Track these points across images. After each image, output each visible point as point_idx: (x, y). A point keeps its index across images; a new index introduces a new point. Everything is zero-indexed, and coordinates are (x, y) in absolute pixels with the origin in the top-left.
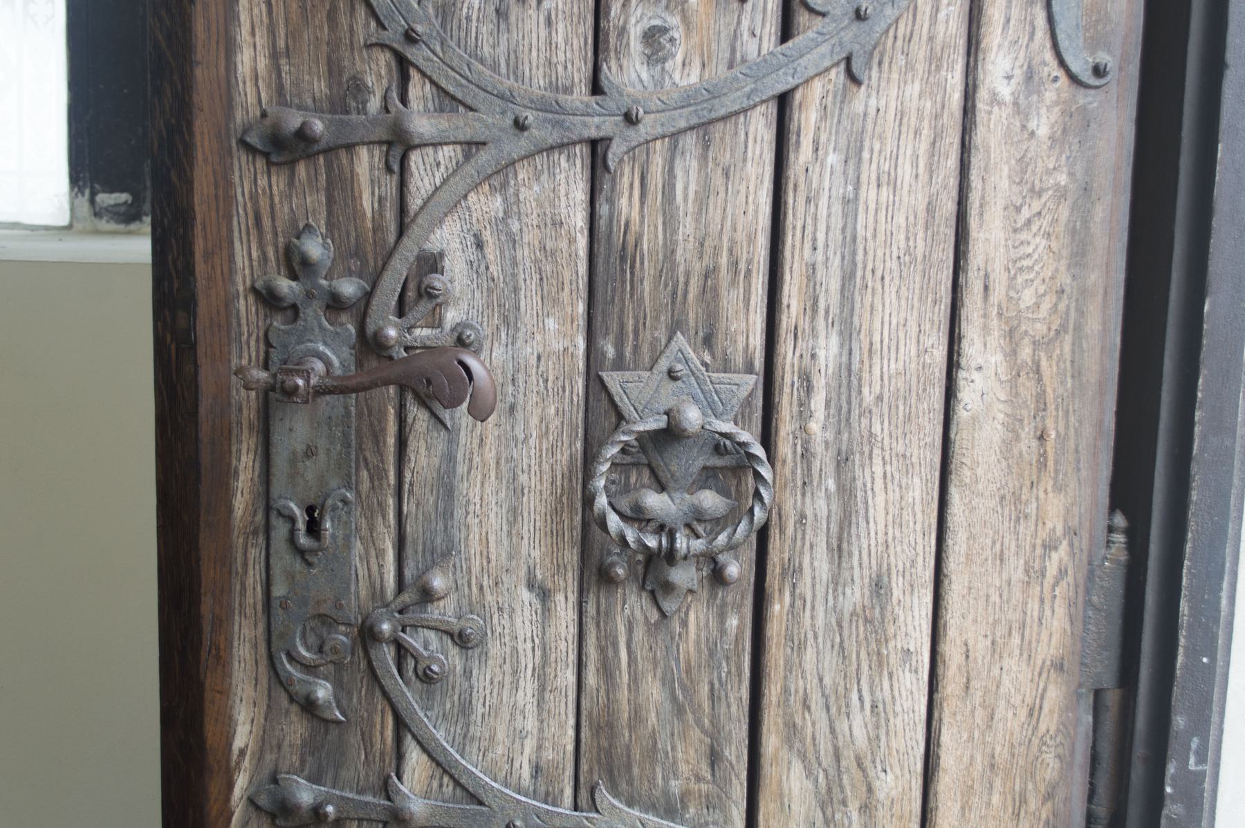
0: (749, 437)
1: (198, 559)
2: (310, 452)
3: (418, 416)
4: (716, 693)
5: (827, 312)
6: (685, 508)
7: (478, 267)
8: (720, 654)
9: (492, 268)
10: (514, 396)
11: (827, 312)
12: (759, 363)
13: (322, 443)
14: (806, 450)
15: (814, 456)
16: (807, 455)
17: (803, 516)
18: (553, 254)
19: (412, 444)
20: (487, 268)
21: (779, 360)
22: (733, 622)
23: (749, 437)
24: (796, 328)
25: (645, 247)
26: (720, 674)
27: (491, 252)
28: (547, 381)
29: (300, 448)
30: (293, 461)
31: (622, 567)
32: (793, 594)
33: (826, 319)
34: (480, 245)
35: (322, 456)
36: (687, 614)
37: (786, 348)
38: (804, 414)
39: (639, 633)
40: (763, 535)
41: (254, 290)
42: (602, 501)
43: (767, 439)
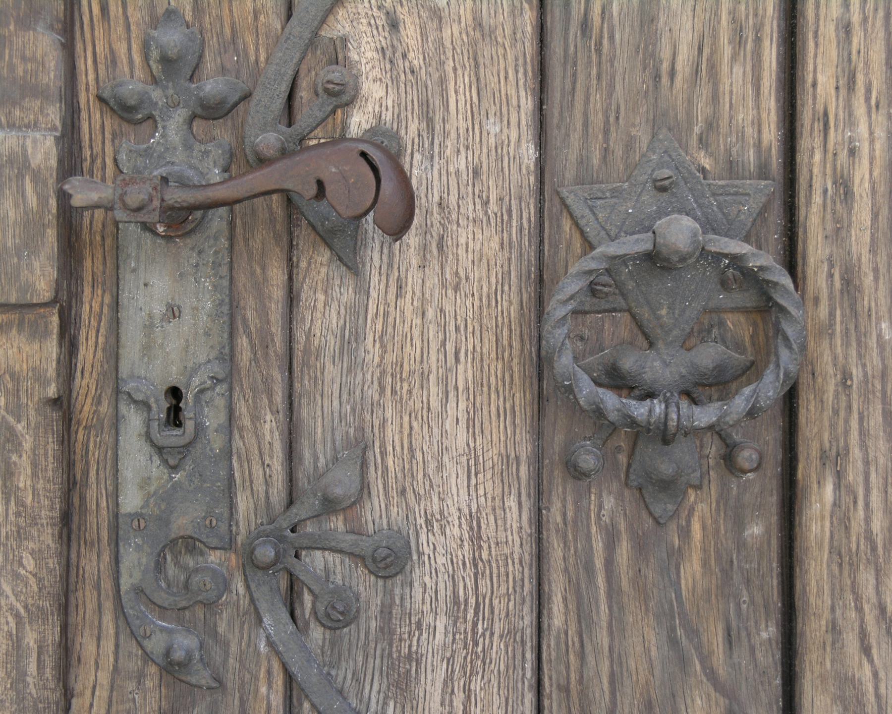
0: (765, 260)
1: (783, 664)
2: (173, 312)
3: (318, 265)
4: (734, 633)
5: (868, 91)
6: (683, 371)
7: (390, 55)
8: (737, 578)
9: (411, 55)
10: (443, 225)
11: (868, 91)
12: (776, 161)
13: (187, 303)
14: (847, 282)
15: (859, 289)
16: (850, 284)
17: (846, 376)
18: (492, 32)
19: (305, 294)
20: (404, 56)
21: (802, 158)
22: (755, 530)
23: (765, 260)
24: (826, 114)
25: (615, 14)
26: (738, 605)
27: (410, 33)
28: (487, 203)
29: (159, 309)
30: (149, 327)
31: (589, 452)
32: (837, 487)
33: (868, 99)
34: (394, 25)
35: (187, 316)
36: (689, 522)
37: (809, 142)
38: (838, 233)
39: (624, 551)
40: (790, 400)
41: (101, 99)
42: (565, 362)
43: (792, 260)
